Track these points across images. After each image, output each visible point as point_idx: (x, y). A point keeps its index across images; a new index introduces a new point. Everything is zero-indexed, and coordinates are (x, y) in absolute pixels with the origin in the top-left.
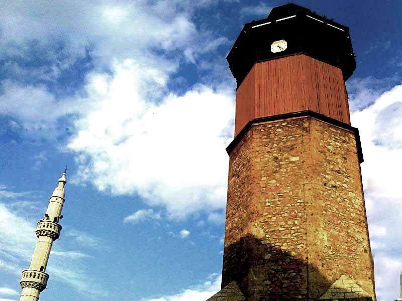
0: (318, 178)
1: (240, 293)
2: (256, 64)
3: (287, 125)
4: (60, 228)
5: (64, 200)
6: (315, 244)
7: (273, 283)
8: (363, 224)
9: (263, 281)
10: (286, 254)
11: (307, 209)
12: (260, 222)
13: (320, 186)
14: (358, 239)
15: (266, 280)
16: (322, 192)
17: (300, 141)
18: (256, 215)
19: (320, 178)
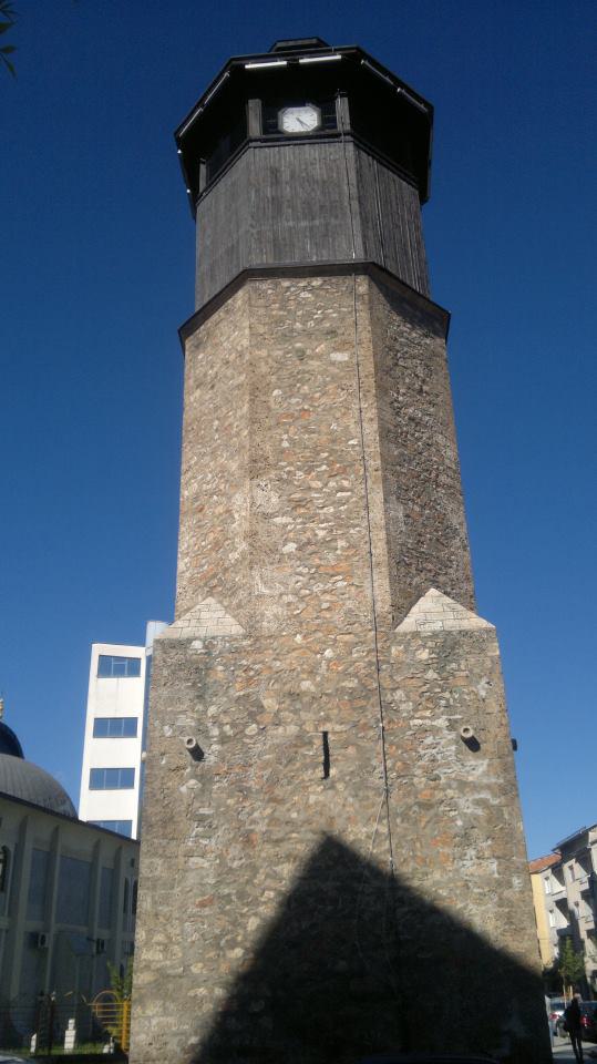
2: (554, 1057)
3: (322, 285)
17: (350, 320)
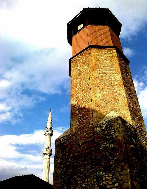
0: (96, 71)
4: (52, 131)
5: (52, 121)
7: (80, 123)
9: (76, 123)
10: (84, 108)
12: (74, 98)
13: (97, 74)
16: (98, 77)
18: (73, 96)
19: (97, 71)
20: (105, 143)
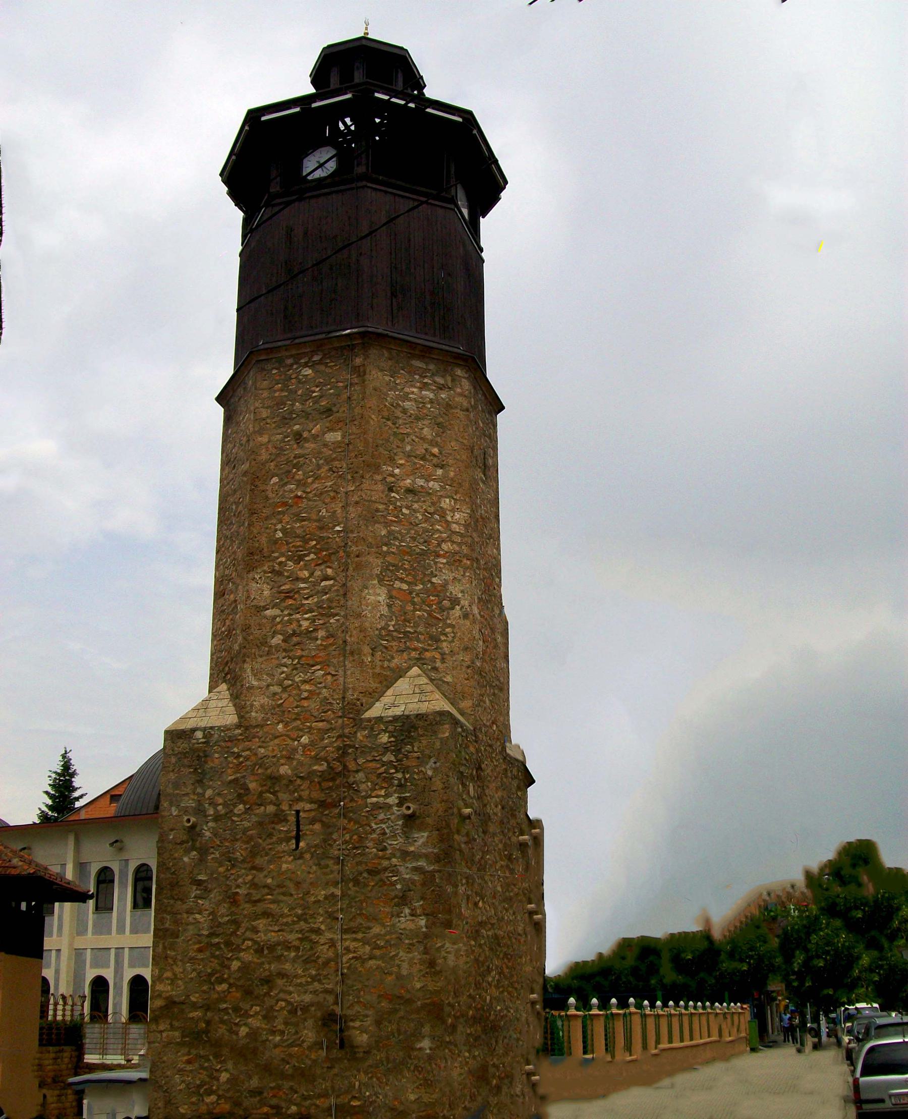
1: (231, 709)
3: (321, 359)
6: (359, 615)
8: (465, 561)
9: (268, 686)
11: (350, 543)
12: (265, 572)
14: (451, 593)
15: (273, 686)
19: (379, 477)
20: (383, 792)
